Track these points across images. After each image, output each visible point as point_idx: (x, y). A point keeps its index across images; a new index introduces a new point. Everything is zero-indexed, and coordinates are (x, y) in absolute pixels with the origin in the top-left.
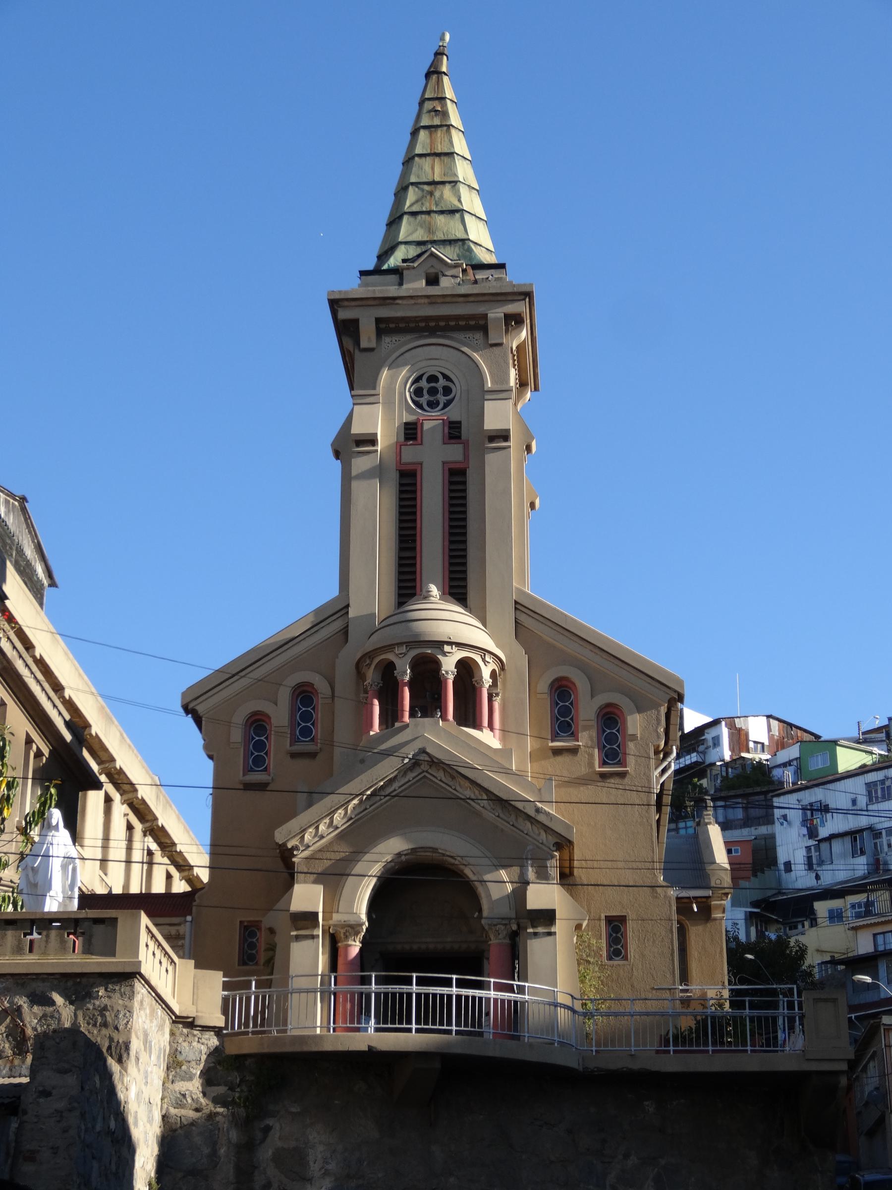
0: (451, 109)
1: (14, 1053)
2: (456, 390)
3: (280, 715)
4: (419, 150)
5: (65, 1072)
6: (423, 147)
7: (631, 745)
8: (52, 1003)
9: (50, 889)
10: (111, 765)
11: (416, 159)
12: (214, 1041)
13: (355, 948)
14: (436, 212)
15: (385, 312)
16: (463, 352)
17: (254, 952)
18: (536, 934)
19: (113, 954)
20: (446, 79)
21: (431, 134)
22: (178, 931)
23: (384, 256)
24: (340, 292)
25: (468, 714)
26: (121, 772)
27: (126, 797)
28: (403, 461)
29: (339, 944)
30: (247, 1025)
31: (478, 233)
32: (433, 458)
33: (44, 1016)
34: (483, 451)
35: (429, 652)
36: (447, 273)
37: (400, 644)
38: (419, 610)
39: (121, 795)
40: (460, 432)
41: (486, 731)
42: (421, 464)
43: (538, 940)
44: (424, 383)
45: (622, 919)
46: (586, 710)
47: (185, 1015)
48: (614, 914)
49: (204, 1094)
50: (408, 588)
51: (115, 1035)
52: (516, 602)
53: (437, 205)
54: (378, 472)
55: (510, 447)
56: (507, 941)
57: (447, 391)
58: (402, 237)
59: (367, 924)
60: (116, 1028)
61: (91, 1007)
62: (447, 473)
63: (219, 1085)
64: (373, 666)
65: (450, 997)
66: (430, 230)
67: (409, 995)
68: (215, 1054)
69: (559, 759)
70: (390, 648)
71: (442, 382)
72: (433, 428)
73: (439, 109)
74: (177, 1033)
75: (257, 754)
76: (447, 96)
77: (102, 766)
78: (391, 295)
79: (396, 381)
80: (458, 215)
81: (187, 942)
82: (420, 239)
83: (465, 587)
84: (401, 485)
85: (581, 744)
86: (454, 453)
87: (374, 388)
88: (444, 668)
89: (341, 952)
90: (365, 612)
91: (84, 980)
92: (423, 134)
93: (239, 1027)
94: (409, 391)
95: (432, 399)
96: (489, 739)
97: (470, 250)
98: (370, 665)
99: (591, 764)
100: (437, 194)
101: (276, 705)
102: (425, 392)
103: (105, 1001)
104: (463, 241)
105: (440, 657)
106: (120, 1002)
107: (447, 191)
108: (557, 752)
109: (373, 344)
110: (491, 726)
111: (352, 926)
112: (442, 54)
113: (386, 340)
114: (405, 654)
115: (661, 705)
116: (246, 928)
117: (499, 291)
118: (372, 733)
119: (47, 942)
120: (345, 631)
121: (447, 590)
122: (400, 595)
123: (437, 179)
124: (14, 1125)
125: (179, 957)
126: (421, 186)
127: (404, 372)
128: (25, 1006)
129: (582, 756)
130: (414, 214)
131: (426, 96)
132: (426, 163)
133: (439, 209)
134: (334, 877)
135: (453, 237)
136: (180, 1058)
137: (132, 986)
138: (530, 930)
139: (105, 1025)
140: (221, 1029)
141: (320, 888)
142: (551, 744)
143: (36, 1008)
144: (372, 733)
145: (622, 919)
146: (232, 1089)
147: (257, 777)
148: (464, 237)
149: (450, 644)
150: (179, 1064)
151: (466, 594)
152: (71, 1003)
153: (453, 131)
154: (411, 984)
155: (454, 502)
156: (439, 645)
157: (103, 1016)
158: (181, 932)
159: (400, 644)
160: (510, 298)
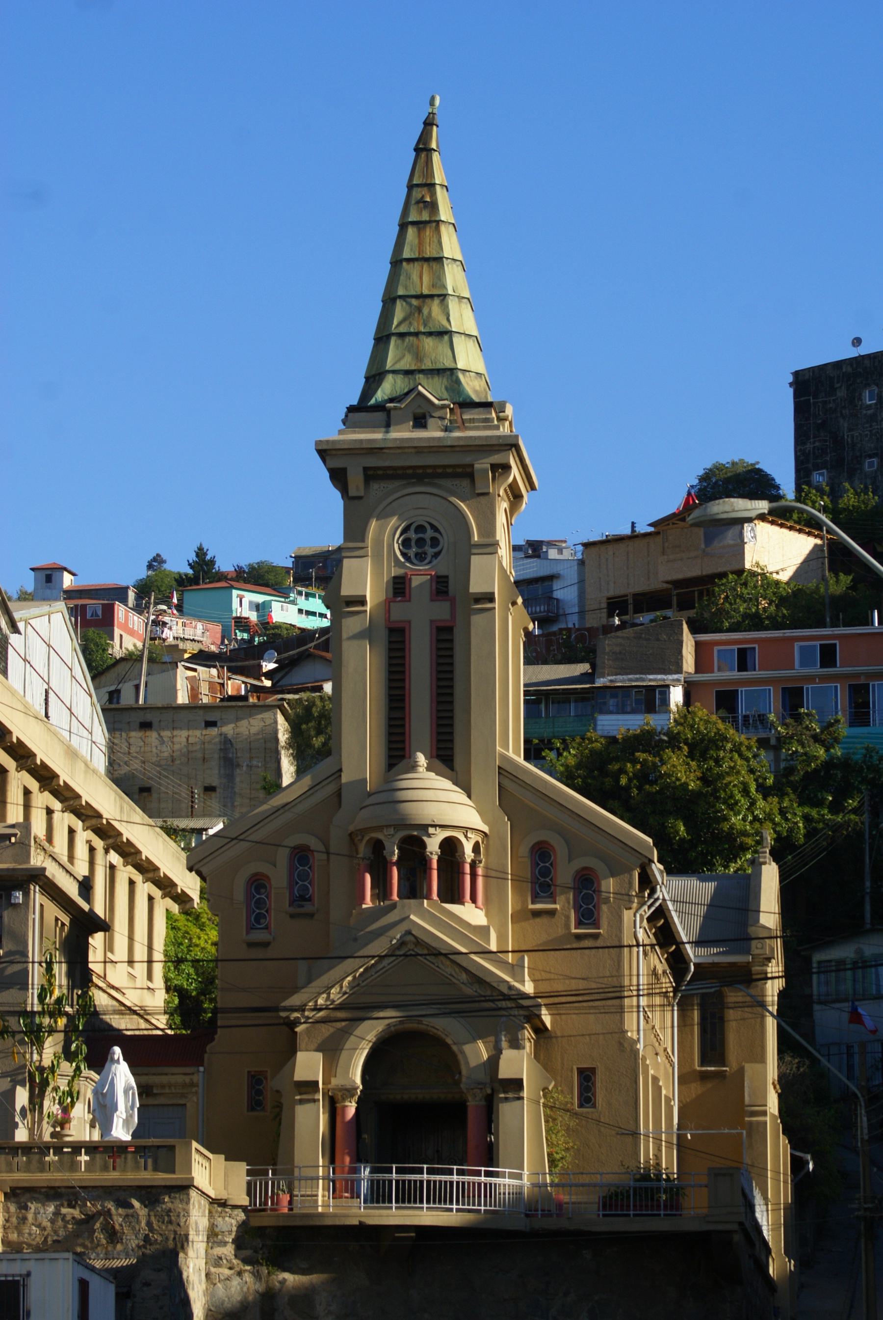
0: (442, 197)
1: (108, 1242)
2: (444, 542)
3: (279, 877)
4: (406, 254)
5: (159, 1270)
6: (411, 250)
7: (604, 908)
8: (132, 1207)
9: (116, 1110)
10: (77, 803)
11: (404, 264)
12: (242, 1216)
13: (351, 1109)
14: (424, 333)
15: (372, 462)
16: (450, 502)
17: (261, 1087)
18: (506, 1099)
19: (174, 1172)
20: (436, 157)
21: (419, 231)
22: (192, 1080)
23: (374, 379)
24: (327, 442)
25: (452, 892)
26: (44, 765)
27: (88, 823)
28: (392, 619)
29: (338, 1105)
30: (266, 1203)
31: (468, 357)
32: (421, 616)
33: (127, 1216)
34: (470, 613)
35: (415, 833)
36: (434, 415)
37: (388, 826)
38: (408, 781)
39: (83, 821)
40: (447, 587)
41: (469, 906)
42: (409, 622)
43: (508, 1104)
44: (412, 535)
45: (593, 1070)
46: (564, 873)
47: (219, 1198)
48: (585, 1066)
49: (236, 1256)
50: (397, 756)
51: (178, 1229)
52: (499, 768)
53: (425, 325)
54: (367, 634)
55: (494, 608)
56: (483, 1103)
57: (435, 542)
58: (389, 365)
59: (361, 1087)
60: (179, 1225)
61: (160, 1209)
62: (434, 631)
63: (246, 1249)
64: (364, 842)
65: (422, 1182)
66: (418, 356)
67: (390, 1181)
68: (243, 1226)
69: (538, 920)
70: (380, 828)
71: (430, 533)
72: (421, 585)
73: (428, 199)
74: (214, 1211)
75: (257, 915)
76: (437, 182)
77: (66, 804)
78: (378, 446)
79: (386, 532)
80: (446, 338)
81: (200, 1090)
82: (407, 367)
83: (452, 749)
84: (390, 642)
85: (558, 906)
86: (441, 611)
87: (363, 541)
88: (429, 849)
89: (339, 1111)
90: (361, 777)
91: (154, 1191)
92: (411, 232)
93: (260, 1205)
94: (397, 542)
95: (420, 551)
96: (472, 914)
97: (458, 382)
98: (361, 840)
99: (567, 926)
100: (425, 311)
101: (275, 866)
102: (413, 543)
103: (170, 1205)
104: (451, 372)
105: (425, 838)
106: (180, 1206)
107: (435, 305)
108: (536, 914)
109: (361, 493)
110: (474, 900)
111: (347, 1090)
112: (432, 124)
113: (375, 486)
114: (393, 835)
115: (633, 870)
116: (253, 1077)
117: (484, 443)
118: (364, 906)
119: (125, 1162)
120: (339, 794)
121: (435, 754)
122: (390, 757)
123: (426, 292)
124: (129, 1305)
125: (212, 1152)
126: (409, 300)
127: (394, 521)
128: (113, 1208)
129: (559, 919)
130: (402, 335)
131: (415, 182)
132: (413, 270)
133: (427, 330)
134: (332, 1050)
135: (441, 366)
136: (217, 1230)
137: (188, 1195)
138: (502, 1095)
139: (170, 1222)
140: (246, 1206)
141: (320, 1056)
142: (531, 906)
143: (120, 1211)
144: (364, 906)
145: (593, 1070)
146: (256, 1252)
147: (259, 936)
148: (452, 366)
149: (435, 826)
150: (216, 1235)
151: (452, 756)
152: (146, 1206)
153: (443, 228)
154: (392, 1173)
155: (448, 653)
156: (424, 827)
157: (169, 1216)
158: (195, 1081)
159: (388, 826)
160: (497, 448)
